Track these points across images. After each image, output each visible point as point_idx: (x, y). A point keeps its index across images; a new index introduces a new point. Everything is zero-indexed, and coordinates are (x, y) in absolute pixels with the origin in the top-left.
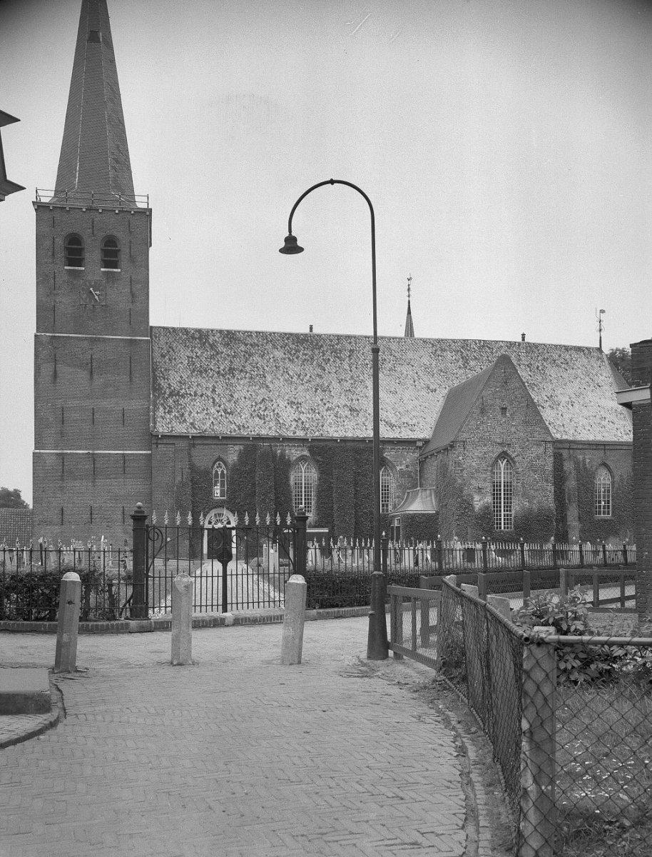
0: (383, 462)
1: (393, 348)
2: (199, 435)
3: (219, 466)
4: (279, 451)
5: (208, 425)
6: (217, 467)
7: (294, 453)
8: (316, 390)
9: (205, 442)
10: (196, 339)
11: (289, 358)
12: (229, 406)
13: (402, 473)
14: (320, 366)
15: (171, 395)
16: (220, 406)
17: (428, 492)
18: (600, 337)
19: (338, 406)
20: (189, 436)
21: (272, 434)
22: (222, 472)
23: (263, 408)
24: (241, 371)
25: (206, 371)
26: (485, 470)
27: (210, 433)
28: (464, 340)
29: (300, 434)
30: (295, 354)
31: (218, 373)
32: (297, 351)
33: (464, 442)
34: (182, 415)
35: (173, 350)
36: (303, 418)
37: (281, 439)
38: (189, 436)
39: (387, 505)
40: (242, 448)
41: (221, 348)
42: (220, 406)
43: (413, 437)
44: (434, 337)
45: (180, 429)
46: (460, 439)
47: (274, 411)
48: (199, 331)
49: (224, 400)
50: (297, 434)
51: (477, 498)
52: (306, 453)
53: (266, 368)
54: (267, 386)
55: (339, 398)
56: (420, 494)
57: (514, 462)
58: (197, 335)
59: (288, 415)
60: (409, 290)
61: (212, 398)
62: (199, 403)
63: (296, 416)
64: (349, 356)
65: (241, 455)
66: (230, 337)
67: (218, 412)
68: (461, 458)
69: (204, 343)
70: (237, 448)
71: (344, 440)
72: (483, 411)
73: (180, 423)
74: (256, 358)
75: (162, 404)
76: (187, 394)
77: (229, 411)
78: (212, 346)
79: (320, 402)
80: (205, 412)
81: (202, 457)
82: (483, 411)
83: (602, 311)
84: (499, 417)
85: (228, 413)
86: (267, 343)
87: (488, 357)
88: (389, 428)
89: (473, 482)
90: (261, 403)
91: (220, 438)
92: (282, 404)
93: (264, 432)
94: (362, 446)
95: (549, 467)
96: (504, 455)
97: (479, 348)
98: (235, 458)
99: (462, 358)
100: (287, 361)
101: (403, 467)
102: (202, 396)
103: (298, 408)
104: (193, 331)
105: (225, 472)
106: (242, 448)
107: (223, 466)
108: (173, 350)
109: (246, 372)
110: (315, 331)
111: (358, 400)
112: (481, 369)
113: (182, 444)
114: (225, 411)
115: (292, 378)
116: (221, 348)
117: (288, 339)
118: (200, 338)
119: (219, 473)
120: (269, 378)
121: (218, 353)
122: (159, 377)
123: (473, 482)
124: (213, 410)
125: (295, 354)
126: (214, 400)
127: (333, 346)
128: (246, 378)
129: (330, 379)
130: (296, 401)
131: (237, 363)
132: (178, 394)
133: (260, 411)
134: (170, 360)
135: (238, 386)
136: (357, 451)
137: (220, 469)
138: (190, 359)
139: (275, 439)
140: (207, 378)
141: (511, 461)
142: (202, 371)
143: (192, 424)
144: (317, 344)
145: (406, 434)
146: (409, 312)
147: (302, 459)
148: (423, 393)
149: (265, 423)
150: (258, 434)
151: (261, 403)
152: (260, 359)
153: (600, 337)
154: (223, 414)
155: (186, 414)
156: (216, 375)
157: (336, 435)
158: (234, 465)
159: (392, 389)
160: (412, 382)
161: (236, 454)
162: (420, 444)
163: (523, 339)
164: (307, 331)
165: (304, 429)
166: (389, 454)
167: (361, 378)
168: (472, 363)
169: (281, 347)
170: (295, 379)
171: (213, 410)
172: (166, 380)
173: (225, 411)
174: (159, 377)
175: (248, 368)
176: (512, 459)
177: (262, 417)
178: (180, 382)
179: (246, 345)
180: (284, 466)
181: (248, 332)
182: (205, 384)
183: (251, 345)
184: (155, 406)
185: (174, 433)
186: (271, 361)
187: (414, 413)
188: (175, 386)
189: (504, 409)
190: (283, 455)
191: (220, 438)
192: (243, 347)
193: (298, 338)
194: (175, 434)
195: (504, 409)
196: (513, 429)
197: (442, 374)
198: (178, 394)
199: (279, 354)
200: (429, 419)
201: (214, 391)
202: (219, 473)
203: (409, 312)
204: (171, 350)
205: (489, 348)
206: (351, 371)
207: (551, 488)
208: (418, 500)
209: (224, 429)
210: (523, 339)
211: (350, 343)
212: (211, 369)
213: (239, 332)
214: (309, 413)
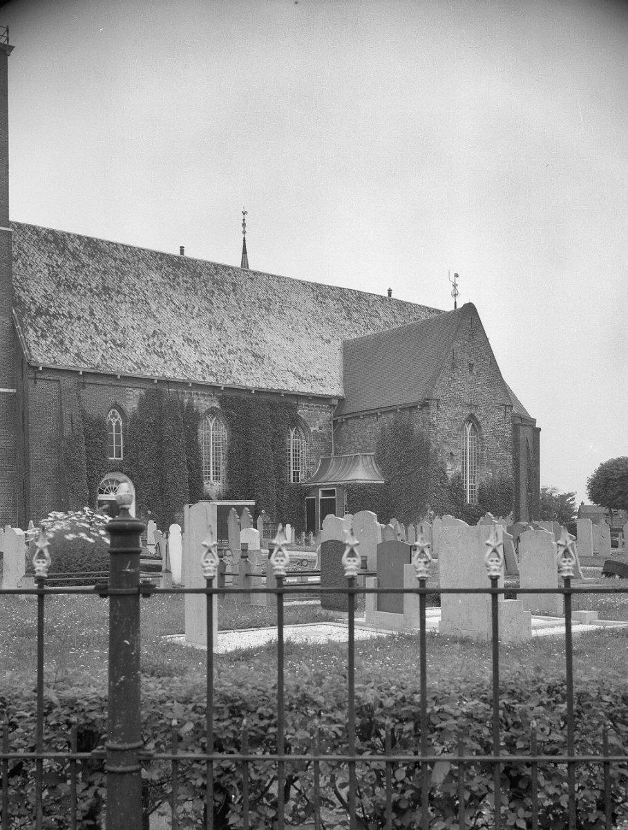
0: (295, 422)
1: (275, 287)
2: (93, 371)
3: (114, 416)
4: (186, 401)
5: (99, 358)
6: (112, 417)
7: (204, 403)
8: (210, 327)
9: (99, 381)
10: (51, 242)
11: (169, 284)
12: (118, 336)
13: (316, 435)
14: (205, 297)
15: (39, 313)
16: (105, 335)
17: (368, 458)
18: (455, 303)
19: (240, 350)
20: (116, 376)
21: (180, 377)
22: (118, 423)
23: (158, 343)
24: (118, 292)
25: (76, 287)
26: (456, 435)
27: (102, 370)
28: (341, 288)
29: (210, 379)
30: (174, 279)
31: (91, 291)
32: (176, 276)
33: (438, 400)
34: (62, 342)
35: (26, 253)
36: (207, 359)
37: (190, 385)
38: (116, 376)
39: (298, 473)
40: (143, 392)
41: (85, 259)
42: (105, 335)
43: (327, 394)
44: (312, 281)
45: (66, 361)
46: (434, 396)
47: (171, 348)
48: (52, 232)
49: (109, 328)
50: (207, 380)
51: (449, 466)
52: (216, 405)
53: (146, 292)
54: (154, 315)
55: (238, 340)
56: (361, 462)
57: (480, 427)
58: (50, 237)
59: (189, 354)
60: (244, 225)
61: (93, 323)
62: (78, 329)
63: (197, 357)
64: (234, 290)
65: (143, 402)
66: (94, 246)
67: (106, 342)
68: (435, 419)
69: (63, 250)
70: (137, 392)
71: (259, 392)
72: (454, 366)
73: (61, 352)
74: (131, 278)
75: (31, 325)
76: (59, 314)
77: (119, 342)
78: (75, 256)
79: (219, 343)
80: (89, 341)
81: (96, 401)
82: (454, 366)
83: (457, 275)
84: (467, 374)
85: (118, 345)
86: (139, 261)
87: (367, 310)
88: (299, 381)
89: (446, 447)
90: (153, 336)
91: (119, 377)
92: (179, 340)
93: (169, 374)
94: (276, 400)
95: (508, 435)
96: (471, 418)
97: (356, 298)
98: (135, 406)
99: (344, 308)
100: (167, 287)
101: (316, 428)
102: (79, 318)
103: (196, 347)
104: (44, 232)
105: (121, 424)
106: (143, 392)
107: (119, 416)
108: (26, 253)
109: (125, 295)
110: (187, 254)
111: (257, 344)
112: (426, 317)
113: (69, 382)
114: (114, 342)
115: (179, 309)
116: (85, 259)
117: (161, 259)
118: (55, 241)
119: (114, 424)
120: (154, 306)
121: (83, 266)
122: (17, 287)
123: (446, 447)
124: (98, 340)
125: (174, 279)
126: (96, 326)
127: (213, 276)
128: (126, 302)
129: (219, 315)
130: (192, 338)
131: (110, 282)
132: (47, 313)
133: (156, 347)
134: (24, 265)
135: (120, 312)
136: (273, 406)
137: (115, 420)
138: (51, 268)
139: (184, 384)
140: (79, 297)
141: (477, 426)
142: (71, 287)
143: (77, 355)
144: (195, 271)
145: (318, 390)
146: (245, 252)
147: (212, 412)
148: (319, 342)
149: (165, 362)
150: (164, 376)
151: (153, 336)
152: (136, 280)
153: (455, 303)
154: (112, 345)
155: (67, 342)
156: (89, 294)
157: (249, 384)
158: (134, 416)
159: (288, 335)
160: (304, 329)
161: (137, 400)
162: (335, 402)
163: (390, 294)
164: (178, 253)
165: (211, 374)
166: (303, 412)
167: (253, 318)
168: (355, 315)
169: (157, 268)
170: (183, 309)
171: (98, 340)
172: (26, 292)
173: (114, 342)
174: (17, 287)
175: (126, 290)
176: (478, 423)
177: (160, 354)
178: (46, 297)
179: (115, 259)
180: (192, 419)
181: (113, 243)
182: (81, 305)
183: (121, 260)
184: (22, 325)
185: (58, 366)
186: (150, 283)
187: (317, 366)
188: (40, 301)
189: (471, 365)
190: (190, 406)
191: (119, 377)
192: (111, 262)
193: (172, 261)
194: (61, 368)
195: (471, 365)
196: (479, 389)
197: (330, 323)
198: (47, 313)
199: (156, 277)
200: (333, 374)
201: (92, 314)
202: (114, 424)
203: (245, 252)
204: (21, 252)
205: (366, 301)
206: (240, 308)
207: (510, 457)
208: (360, 467)
209: (121, 365)
210: (390, 294)
211: (229, 275)
212: (81, 286)
213: (102, 241)
214: (212, 355)
